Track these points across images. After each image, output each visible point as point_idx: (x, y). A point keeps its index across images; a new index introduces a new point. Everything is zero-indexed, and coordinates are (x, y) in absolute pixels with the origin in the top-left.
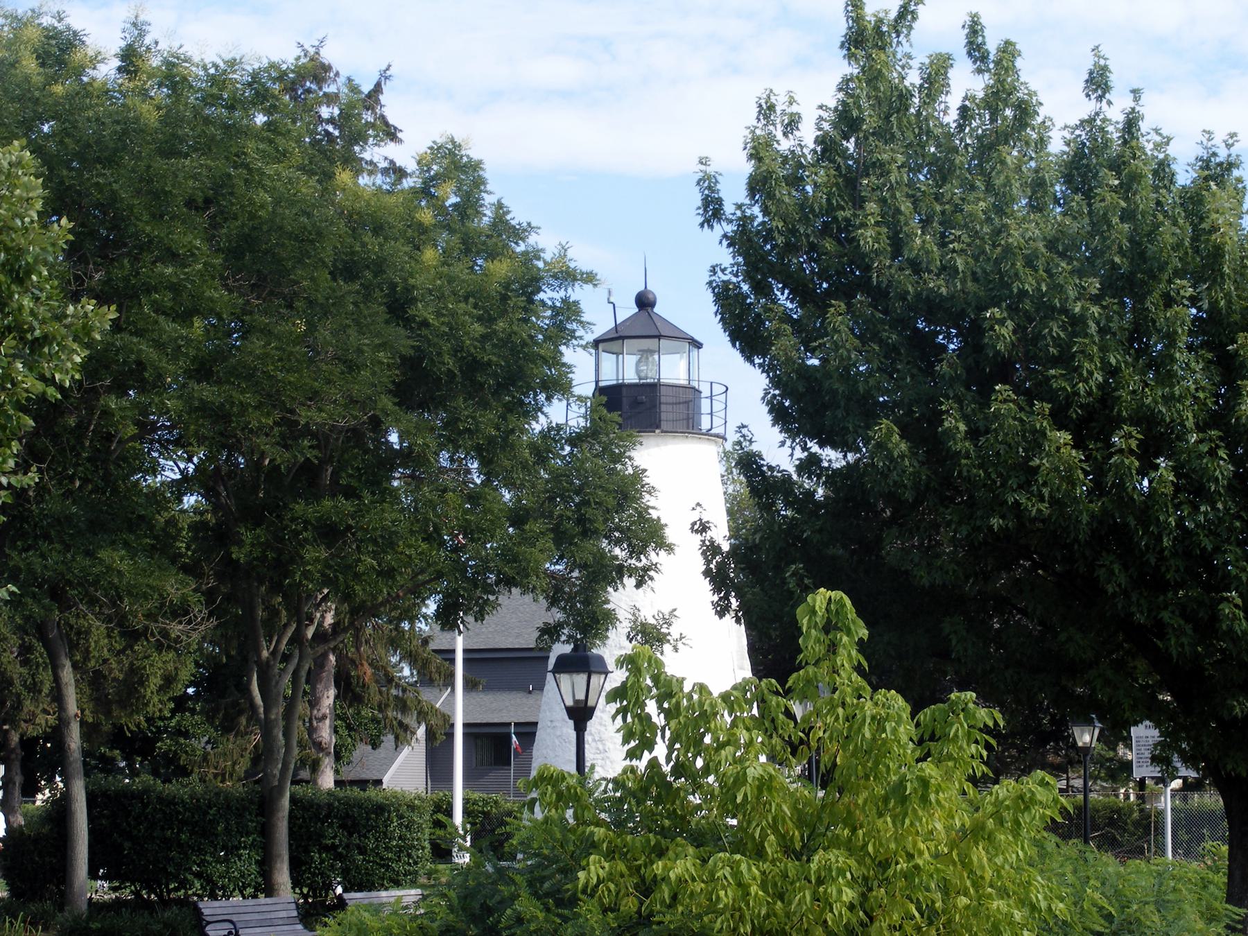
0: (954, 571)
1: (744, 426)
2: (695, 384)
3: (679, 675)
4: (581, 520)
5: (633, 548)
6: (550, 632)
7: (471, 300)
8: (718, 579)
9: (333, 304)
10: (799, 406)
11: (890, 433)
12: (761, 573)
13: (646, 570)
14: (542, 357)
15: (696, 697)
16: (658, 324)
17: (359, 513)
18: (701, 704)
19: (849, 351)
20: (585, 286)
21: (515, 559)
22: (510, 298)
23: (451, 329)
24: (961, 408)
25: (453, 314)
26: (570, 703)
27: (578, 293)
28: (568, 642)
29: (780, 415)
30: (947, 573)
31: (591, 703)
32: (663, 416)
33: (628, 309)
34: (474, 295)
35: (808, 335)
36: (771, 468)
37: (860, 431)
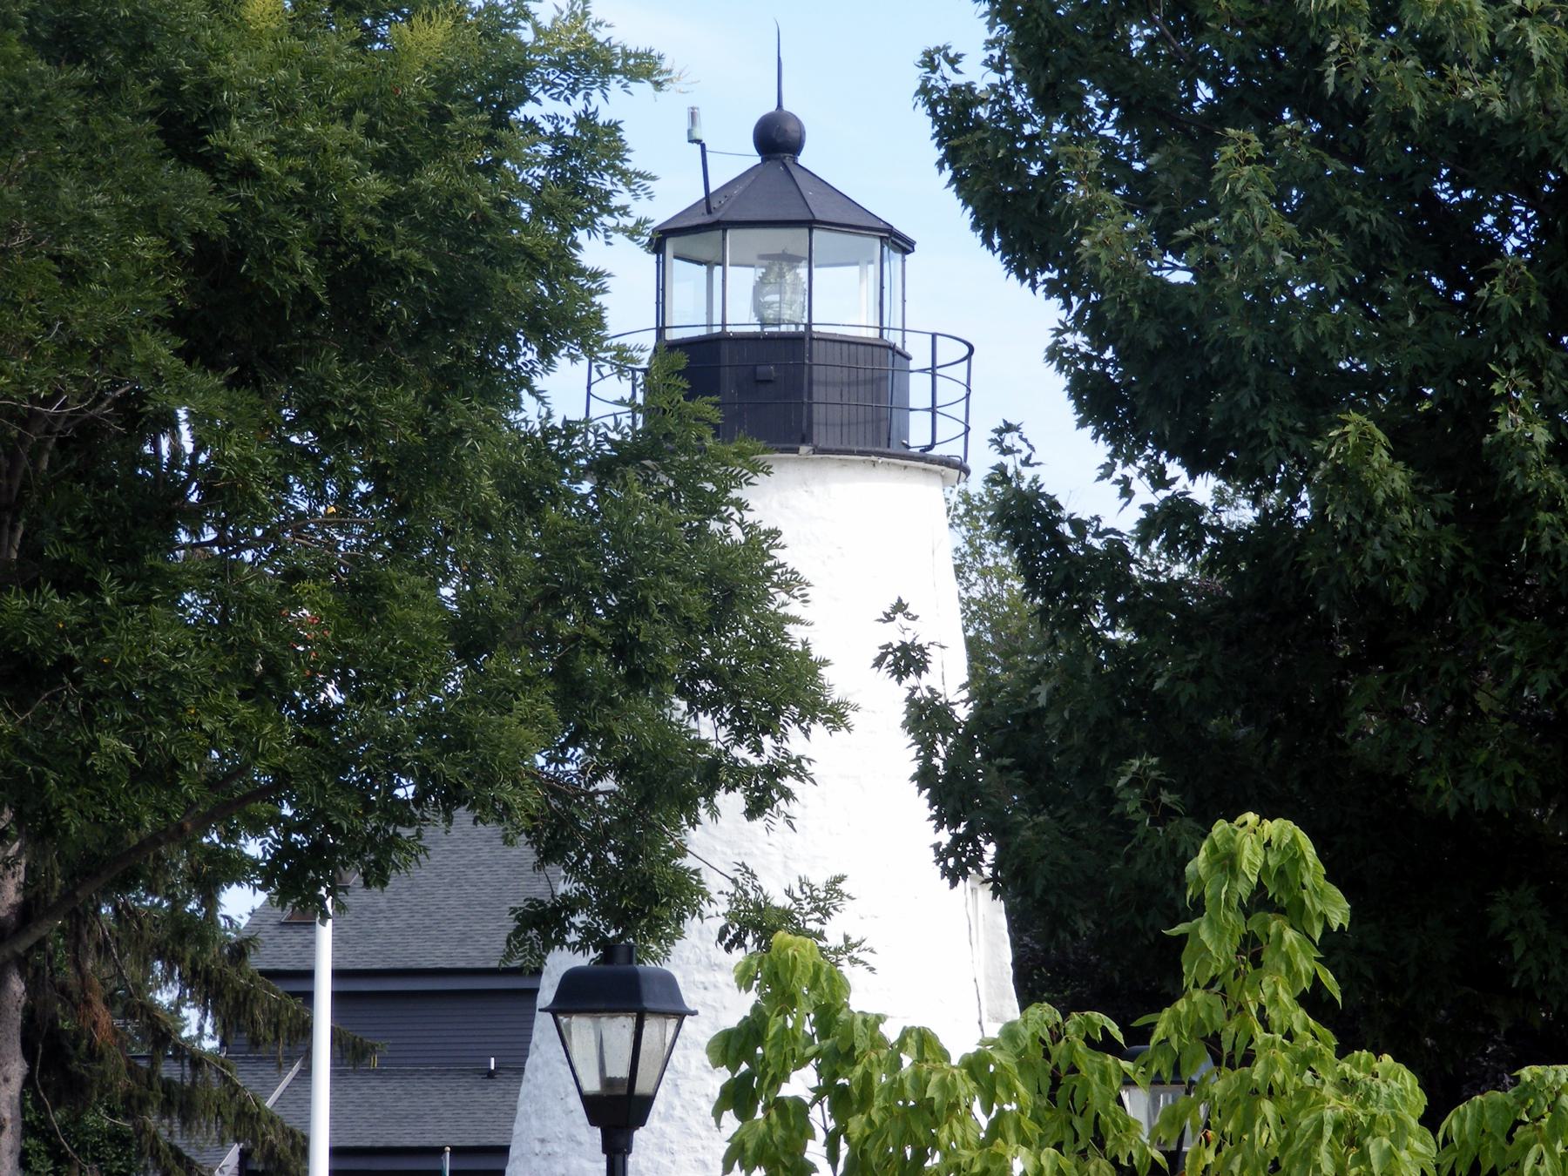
0: (1518, 778)
1: (1009, 428)
2: (893, 338)
3: (872, 1009)
4: (624, 649)
5: (746, 718)
6: (543, 922)
7: (360, 116)
8: (950, 794)
9: (27, 117)
10: (1139, 385)
11: (1366, 445)
12: (1064, 777)
13: (774, 772)
14: (531, 256)
15: (907, 1061)
16: (809, 194)
17: (93, 627)
18: (920, 1083)
19: (1268, 250)
20: (633, 86)
21: (462, 739)
22: (449, 116)
23: (310, 186)
24: (1538, 389)
25: (316, 149)
26: (592, 1085)
27: (616, 103)
28: (582, 946)
29: (1096, 401)
30: (1500, 781)
31: (642, 1087)
32: (819, 413)
33: (737, 156)
34: (371, 104)
35: (1169, 214)
36: (1079, 526)
37: (1294, 442)
